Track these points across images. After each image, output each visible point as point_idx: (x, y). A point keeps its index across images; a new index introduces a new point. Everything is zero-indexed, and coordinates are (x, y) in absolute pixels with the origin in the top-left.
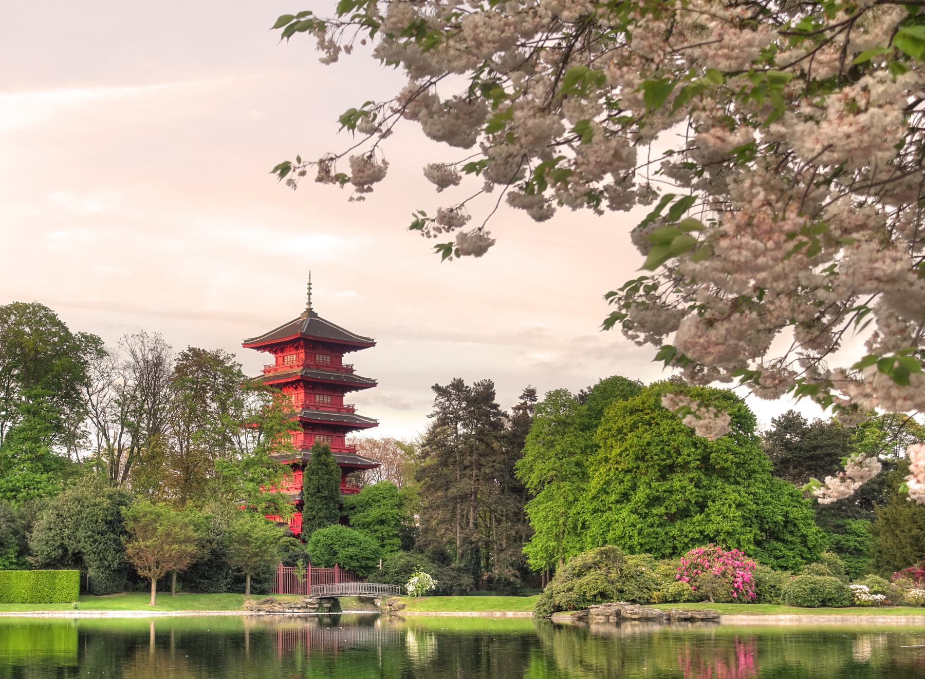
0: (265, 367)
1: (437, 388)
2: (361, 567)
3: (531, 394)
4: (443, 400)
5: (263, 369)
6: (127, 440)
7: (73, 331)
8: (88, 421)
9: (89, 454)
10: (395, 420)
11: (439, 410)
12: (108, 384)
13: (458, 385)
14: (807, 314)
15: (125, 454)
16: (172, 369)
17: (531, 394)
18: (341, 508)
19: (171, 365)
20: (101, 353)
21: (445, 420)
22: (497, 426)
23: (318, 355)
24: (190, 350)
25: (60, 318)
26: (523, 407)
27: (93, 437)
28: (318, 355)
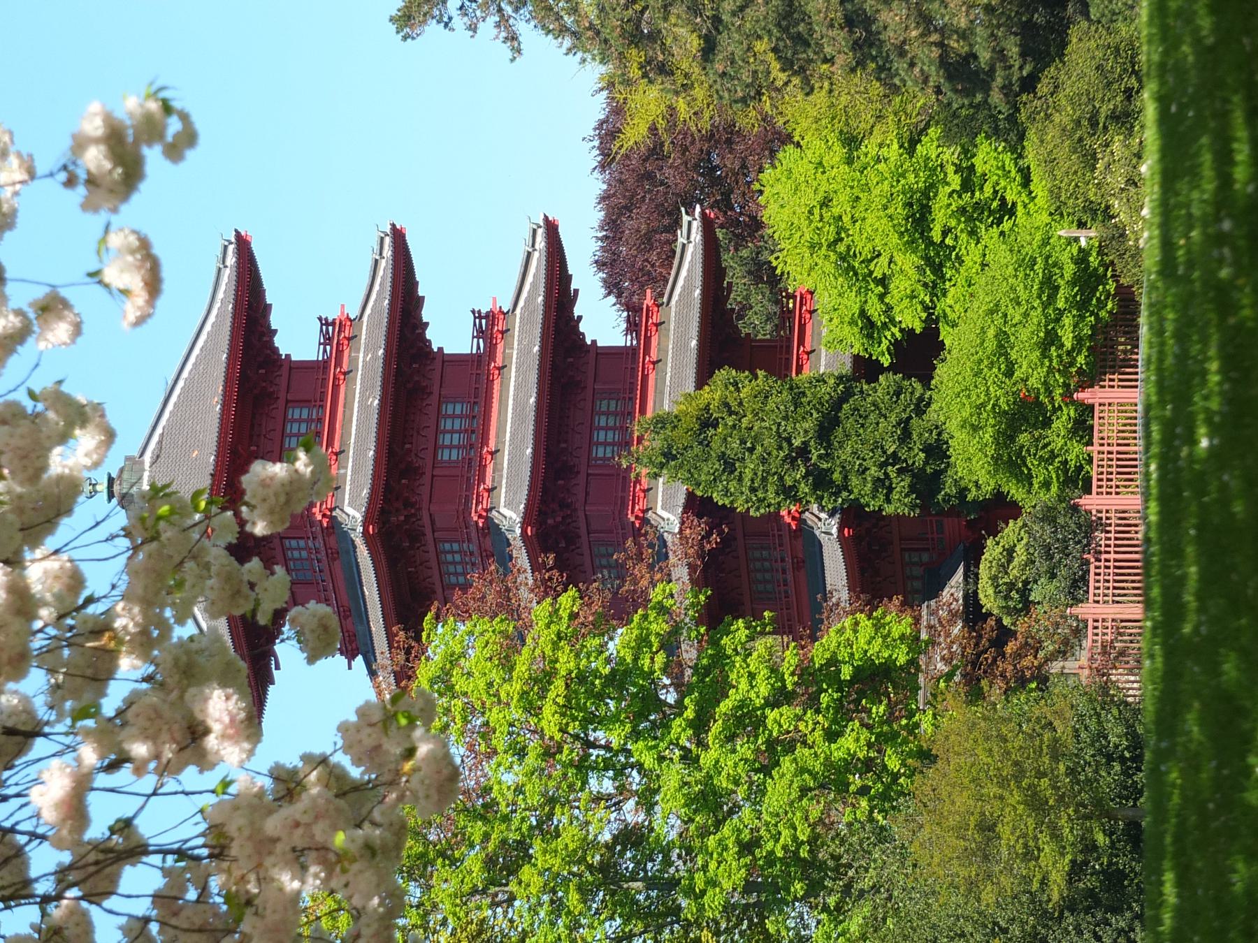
2: (1082, 306)
18: (866, 368)
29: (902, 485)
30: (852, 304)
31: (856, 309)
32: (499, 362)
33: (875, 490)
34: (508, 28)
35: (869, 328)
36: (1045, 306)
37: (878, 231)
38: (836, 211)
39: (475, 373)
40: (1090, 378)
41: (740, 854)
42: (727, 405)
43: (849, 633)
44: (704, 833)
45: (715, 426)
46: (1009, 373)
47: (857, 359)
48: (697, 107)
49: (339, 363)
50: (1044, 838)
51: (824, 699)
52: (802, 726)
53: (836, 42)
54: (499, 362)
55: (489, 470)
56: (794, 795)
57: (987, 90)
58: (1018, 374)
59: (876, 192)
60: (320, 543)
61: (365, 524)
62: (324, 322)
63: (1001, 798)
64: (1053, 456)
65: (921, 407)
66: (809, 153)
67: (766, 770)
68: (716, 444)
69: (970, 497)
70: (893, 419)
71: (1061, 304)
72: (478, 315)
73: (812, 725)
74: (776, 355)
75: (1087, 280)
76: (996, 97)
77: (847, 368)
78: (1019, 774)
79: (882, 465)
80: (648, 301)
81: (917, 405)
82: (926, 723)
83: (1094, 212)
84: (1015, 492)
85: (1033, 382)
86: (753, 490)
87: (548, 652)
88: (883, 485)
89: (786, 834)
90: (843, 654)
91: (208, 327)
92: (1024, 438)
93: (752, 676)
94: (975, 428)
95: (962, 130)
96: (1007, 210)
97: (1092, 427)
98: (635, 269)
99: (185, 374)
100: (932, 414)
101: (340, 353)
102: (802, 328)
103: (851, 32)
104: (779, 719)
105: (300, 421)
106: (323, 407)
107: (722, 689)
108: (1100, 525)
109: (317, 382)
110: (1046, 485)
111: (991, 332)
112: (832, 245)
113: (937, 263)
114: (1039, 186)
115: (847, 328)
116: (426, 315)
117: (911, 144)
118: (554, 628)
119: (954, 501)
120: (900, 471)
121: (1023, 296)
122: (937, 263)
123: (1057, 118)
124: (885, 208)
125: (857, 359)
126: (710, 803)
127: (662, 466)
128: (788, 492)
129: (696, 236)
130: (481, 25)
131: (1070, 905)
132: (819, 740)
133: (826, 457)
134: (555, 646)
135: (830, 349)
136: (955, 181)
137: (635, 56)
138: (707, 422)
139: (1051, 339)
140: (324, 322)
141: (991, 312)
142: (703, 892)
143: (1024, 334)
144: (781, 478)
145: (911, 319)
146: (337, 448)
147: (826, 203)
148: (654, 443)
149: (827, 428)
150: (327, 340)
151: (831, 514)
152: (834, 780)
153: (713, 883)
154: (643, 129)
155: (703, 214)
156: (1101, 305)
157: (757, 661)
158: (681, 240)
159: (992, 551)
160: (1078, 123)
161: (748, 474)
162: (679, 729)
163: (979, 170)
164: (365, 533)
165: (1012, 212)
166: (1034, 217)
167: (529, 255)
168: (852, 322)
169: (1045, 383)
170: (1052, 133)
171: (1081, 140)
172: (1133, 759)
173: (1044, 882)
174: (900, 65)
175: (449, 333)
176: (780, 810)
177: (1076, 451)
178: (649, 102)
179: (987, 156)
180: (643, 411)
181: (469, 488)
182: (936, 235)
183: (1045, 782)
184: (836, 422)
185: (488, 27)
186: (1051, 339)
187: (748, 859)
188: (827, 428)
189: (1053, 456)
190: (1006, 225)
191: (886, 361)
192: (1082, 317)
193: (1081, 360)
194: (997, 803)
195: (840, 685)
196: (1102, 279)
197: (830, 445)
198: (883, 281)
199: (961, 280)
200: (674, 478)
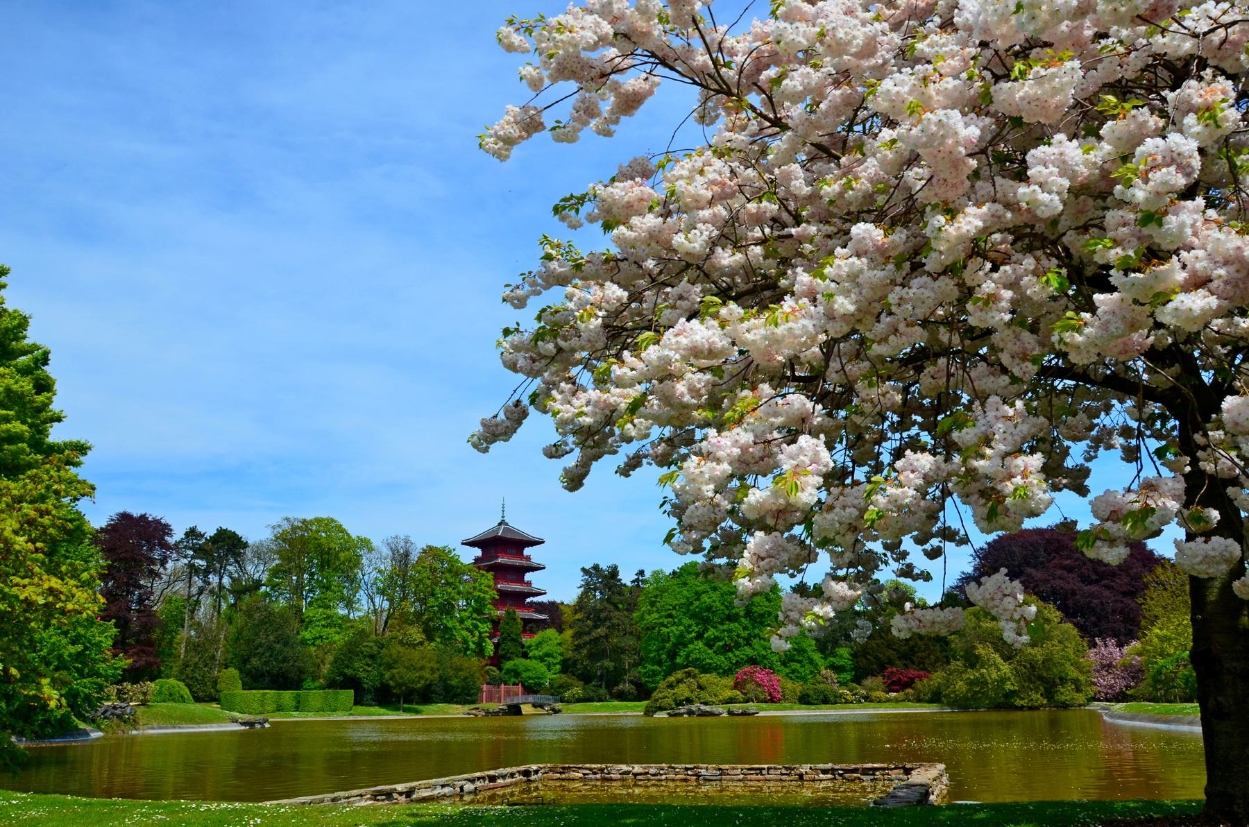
1: (583, 569)
3: (642, 573)
6: (386, 604)
7: (353, 536)
8: (361, 592)
9: (361, 614)
10: (558, 583)
12: (373, 568)
13: (596, 567)
14: (1226, 561)
15: (385, 614)
17: (642, 573)
18: (523, 646)
19: (414, 557)
20: (370, 550)
21: (588, 589)
22: (620, 594)
23: (504, 551)
25: (344, 527)
26: (637, 580)
27: (364, 602)
28: (504, 551)
35: (529, 647)
37: (545, 649)
40: (523, 685)
48: (565, 618)
53: (581, 641)
73: (475, 639)
74: (524, 631)
75: (540, 685)
98: (540, 607)
122: (541, 659)
126: (462, 621)
135: (526, 640)
149: (513, 640)
152: (465, 641)
157: (486, 628)
162: (475, 615)
166: (550, 675)
175: (528, 577)
176: (461, 634)
188: (513, 640)
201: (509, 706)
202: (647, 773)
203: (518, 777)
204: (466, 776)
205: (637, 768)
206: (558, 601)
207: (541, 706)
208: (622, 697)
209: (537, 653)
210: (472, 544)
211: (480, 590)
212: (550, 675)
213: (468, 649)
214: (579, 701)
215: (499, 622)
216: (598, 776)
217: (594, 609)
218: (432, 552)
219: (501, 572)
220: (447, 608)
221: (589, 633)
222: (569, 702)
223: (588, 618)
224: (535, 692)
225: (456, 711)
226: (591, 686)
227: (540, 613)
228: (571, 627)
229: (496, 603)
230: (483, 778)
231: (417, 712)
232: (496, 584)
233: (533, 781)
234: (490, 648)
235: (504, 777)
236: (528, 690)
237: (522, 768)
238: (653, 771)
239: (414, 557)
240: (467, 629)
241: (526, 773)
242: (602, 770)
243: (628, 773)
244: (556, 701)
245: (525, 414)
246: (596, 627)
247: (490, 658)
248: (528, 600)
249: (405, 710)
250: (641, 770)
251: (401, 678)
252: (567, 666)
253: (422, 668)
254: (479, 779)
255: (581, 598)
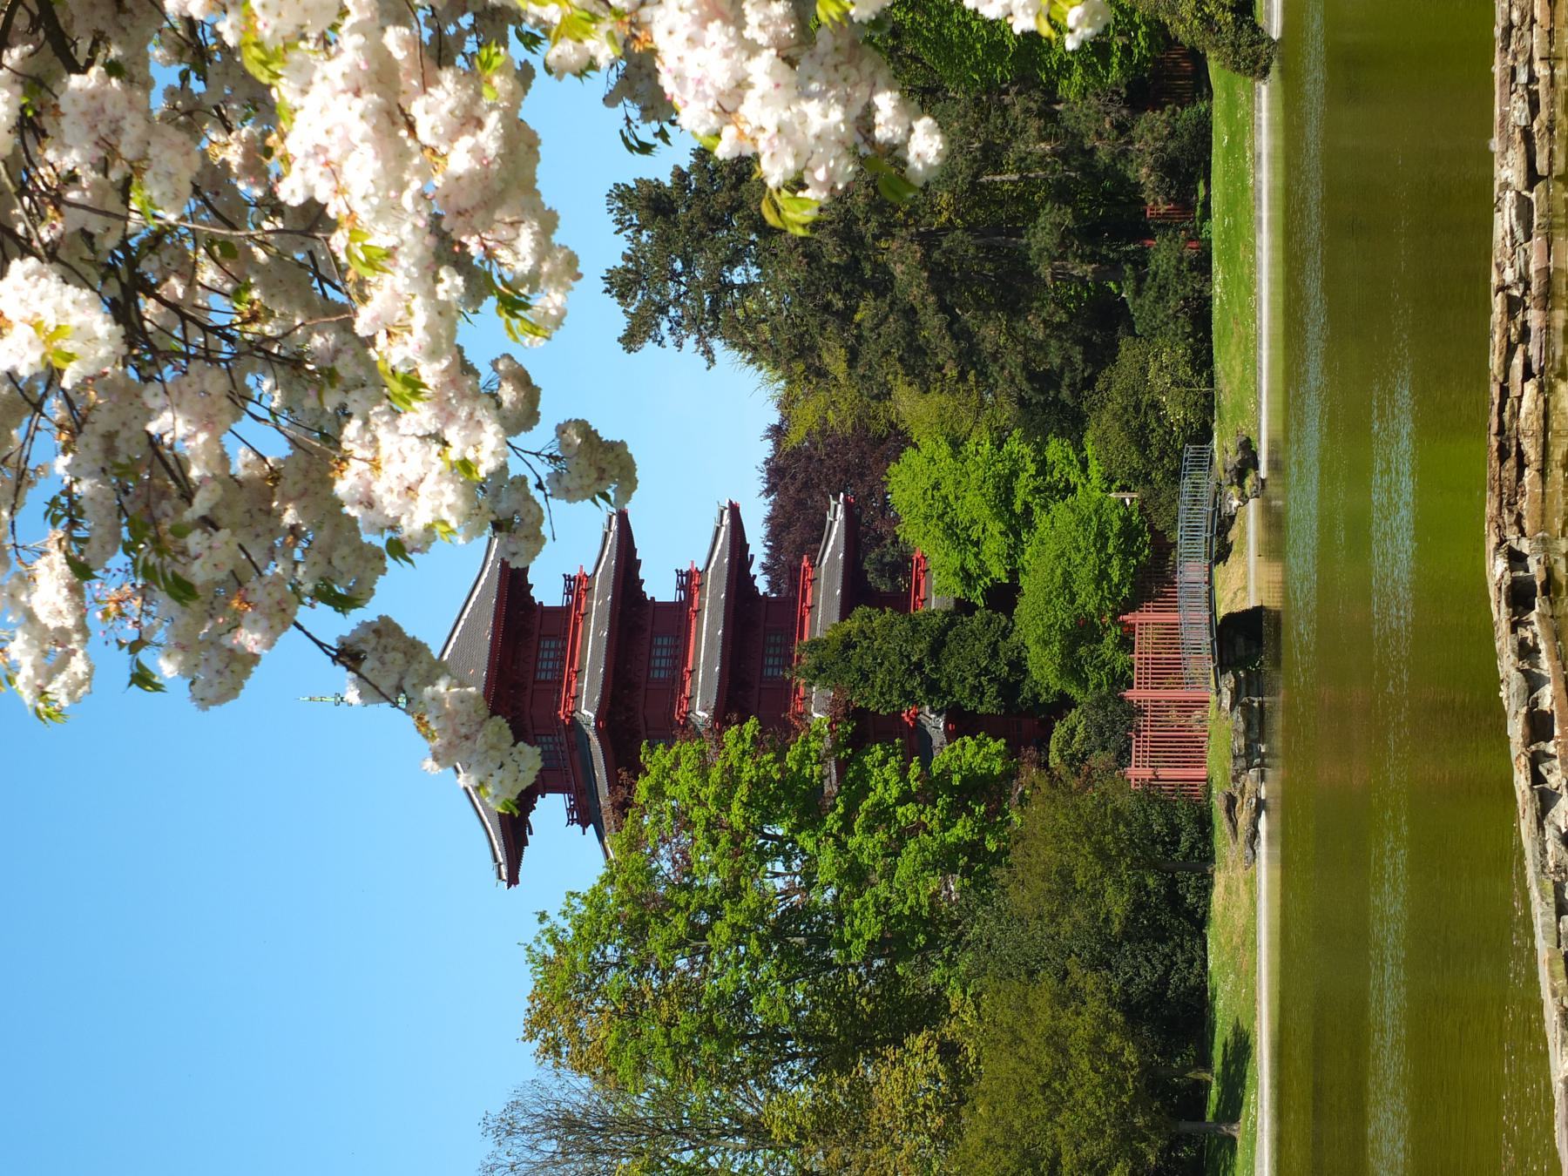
0: (571, 822)
1: (631, 340)
2: (1126, 553)
4: (665, 325)
5: (577, 827)
11: (694, 337)
16: (585, 1082)
19: (576, 1090)
21: (716, 318)
24: (531, 1035)
29: (991, 690)
30: (955, 560)
31: (958, 564)
32: (696, 607)
33: (971, 694)
34: (705, 344)
35: (968, 578)
36: (1099, 552)
37: (974, 506)
38: (943, 492)
39: (678, 616)
40: (1131, 605)
41: (878, 913)
42: (863, 632)
43: (958, 751)
44: (850, 898)
45: (854, 648)
46: (1072, 601)
47: (958, 601)
49: (578, 607)
50: (1108, 881)
51: (940, 802)
52: (923, 817)
53: (945, 350)
54: (696, 607)
55: (688, 684)
56: (918, 867)
57: (1058, 388)
58: (1079, 601)
59: (973, 476)
60: (563, 738)
61: (597, 721)
62: (567, 578)
63: (1076, 850)
64: (1104, 664)
65: (1006, 633)
66: (924, 451)
67: (897, 854)
68: (855, 661)
69: (1041, 700)
70: (985, 642)
71: (1110, 551)
72: (680, 573)
74: (900, 602)
75: (1129, 533)
76: (1065, 394)
77: (952, 606)
78: (1089, 831)
79: (977, 676)
80: (805, 564)
81: (1003, 632)
82: (1016, 818)
83: (1137, 478)
84: (1073, 691)
85: (1090, 608)
86: (882, 694)
87: (736, 764)
88: (977, 690)
89: (911, 898)
90: (954, 766)
91: (482, 581)
92: (1082, 651)
93: (886, 782)
94: (1046, 643)
95: (1036, 432)
96: (1070, 489)
97: (1133, 643)
98: (795, 527)
99: (465, 616)
100: (1014, 638)
101: (579, 601)
102: (918, 583)
103: (958, 343)
104: (906, 813)
105: (549, 650)
106: (566, 639)
107: (865, 790)
108: (1140, 712)
109: (562, 622)
110: (1099, 686)
111: (1059, 571)
112: (940, 517)
113: (1019, 525)
114: (1094, 469)
115: (951, 580)
116: (642, 575)
117: (999, 444)
118: (740, 746)
119: (1030, 704)
120: (990, 681)
121: (1082, 544)
122: (1019, 525)
123: (1110, 406)
124: (980, 488)
125: (958, 601)
126: (856, 876)
127: (815, 677)
128: (908, 696)
129: (840, 516)
130: (685, 341)
131: (1127, 936)
132: (937, 829)
133: (936, 670)
134: (741, 760)
135: (938, 592)
136: (1032, 469)
137: (799, 367)
138: (848, 645)
139: (1103, 575)
140: (567, 578)
141: (1058, 557)
142: (850, 942)
143: (1083, 572)
144: (902, 686)
145: (999, 572)
146: (576, 668)
147: (936, 486)
148: (808, 661)
149: (937, 648)
150: (569, 592)
151: (939, 714)
152: (945, 861)
153: (858, 935)
154: (803, 432)
155: (845, 499)
156: (1140, 551)
158: (829, 519)
159: (1059, 731)
160: (1125, 409)
161: (879, 682)
162: (832, 821)
163: (1049, 461)
164: (597, 727)
165: (1074, 491)
166: (1091, 491)
167: (718, 530)
168: (955, 574)
169: (1098, 609)
170: (1106, 417)
171: (1128, 421)
172: (1171, 843)
173: (1107, 920)
174: (993, 369)
175: (659, 586)
176: (913, 883)
177: (1121, 659)
178: (808, 415)
179: (1055, 450)
180: (801, 637)
181: (674, 697)
182: (1018, 507)
183: (1109, 838)
184: (943, 644)
185: (690, 342)
186: (1103, 575)
187: (883, 917)
188: (937, 648)
189: (1104, 664)
190: (1070, 500)
191: (980, 602)
192: (1126, 560)
193: (1125, 591)
194: (1073, 855)
195: (951, 790)
196: (1141, 533)
197: (938, 661)
198: (977, 544)
199: (1035, 542)
200: (824, 686)
201: (1222, 667)
202: (1527, 136)
203: (1536, 628)
204: (1526, 826)
205: (1509, 170)
206: (766, 449)
207: (1224, 524)
208: (1188, 166)
209: (994, 546)
210: (514, 832)
211: (724, 803)
212: (1091, 491)
213: (974, 849)
214: (1202, 361)
215: (860, 715)
216: (1534, 318)
217: (806, 291)
218: (558, 1009)
219: (640, 709)
220: (797, 938)
221: (910, 313)
222: (1208, 406)
223: (846, 316)
224: (1163, 549)
225: (1247, 896)
226: (1140, 307)
227: (819, 530)
228: (885, 394)
229: (780, 726)
230: (1536, 760)
231: (1241, 1049)
232: (687, 729)
233: (1549, 571)
234: (976, 755)
235: (1533, 682)
236: (1152, 577)
237: (1500, 614)
238: (1518, 111)
239: (576, 1090)
240: (893, 850)
241: (1520, 597)
242: (1513, 306)
243: (1524, 209)
244: (1204, 462)
245: (385, 629)
246: (883, 285)
247: (1012, 751)
248: (762, 584)
249: (1233, 1105)
250: (1516, 156)
251: (1097, 1132)
252: (1054, 410)
253: (1056, 1041)
254: (1537, 778)
255: (756, 352)
